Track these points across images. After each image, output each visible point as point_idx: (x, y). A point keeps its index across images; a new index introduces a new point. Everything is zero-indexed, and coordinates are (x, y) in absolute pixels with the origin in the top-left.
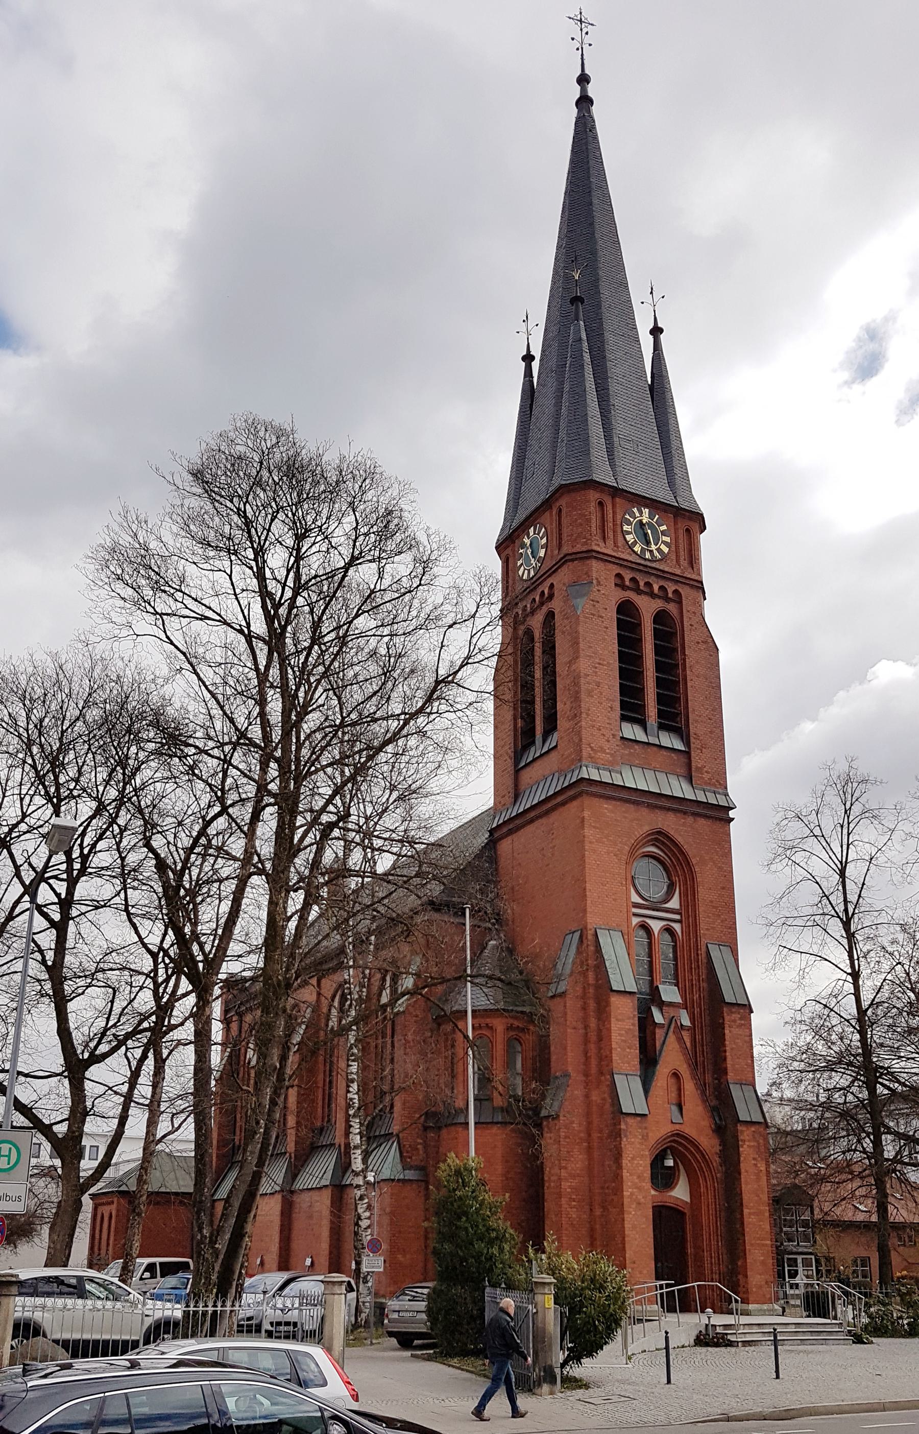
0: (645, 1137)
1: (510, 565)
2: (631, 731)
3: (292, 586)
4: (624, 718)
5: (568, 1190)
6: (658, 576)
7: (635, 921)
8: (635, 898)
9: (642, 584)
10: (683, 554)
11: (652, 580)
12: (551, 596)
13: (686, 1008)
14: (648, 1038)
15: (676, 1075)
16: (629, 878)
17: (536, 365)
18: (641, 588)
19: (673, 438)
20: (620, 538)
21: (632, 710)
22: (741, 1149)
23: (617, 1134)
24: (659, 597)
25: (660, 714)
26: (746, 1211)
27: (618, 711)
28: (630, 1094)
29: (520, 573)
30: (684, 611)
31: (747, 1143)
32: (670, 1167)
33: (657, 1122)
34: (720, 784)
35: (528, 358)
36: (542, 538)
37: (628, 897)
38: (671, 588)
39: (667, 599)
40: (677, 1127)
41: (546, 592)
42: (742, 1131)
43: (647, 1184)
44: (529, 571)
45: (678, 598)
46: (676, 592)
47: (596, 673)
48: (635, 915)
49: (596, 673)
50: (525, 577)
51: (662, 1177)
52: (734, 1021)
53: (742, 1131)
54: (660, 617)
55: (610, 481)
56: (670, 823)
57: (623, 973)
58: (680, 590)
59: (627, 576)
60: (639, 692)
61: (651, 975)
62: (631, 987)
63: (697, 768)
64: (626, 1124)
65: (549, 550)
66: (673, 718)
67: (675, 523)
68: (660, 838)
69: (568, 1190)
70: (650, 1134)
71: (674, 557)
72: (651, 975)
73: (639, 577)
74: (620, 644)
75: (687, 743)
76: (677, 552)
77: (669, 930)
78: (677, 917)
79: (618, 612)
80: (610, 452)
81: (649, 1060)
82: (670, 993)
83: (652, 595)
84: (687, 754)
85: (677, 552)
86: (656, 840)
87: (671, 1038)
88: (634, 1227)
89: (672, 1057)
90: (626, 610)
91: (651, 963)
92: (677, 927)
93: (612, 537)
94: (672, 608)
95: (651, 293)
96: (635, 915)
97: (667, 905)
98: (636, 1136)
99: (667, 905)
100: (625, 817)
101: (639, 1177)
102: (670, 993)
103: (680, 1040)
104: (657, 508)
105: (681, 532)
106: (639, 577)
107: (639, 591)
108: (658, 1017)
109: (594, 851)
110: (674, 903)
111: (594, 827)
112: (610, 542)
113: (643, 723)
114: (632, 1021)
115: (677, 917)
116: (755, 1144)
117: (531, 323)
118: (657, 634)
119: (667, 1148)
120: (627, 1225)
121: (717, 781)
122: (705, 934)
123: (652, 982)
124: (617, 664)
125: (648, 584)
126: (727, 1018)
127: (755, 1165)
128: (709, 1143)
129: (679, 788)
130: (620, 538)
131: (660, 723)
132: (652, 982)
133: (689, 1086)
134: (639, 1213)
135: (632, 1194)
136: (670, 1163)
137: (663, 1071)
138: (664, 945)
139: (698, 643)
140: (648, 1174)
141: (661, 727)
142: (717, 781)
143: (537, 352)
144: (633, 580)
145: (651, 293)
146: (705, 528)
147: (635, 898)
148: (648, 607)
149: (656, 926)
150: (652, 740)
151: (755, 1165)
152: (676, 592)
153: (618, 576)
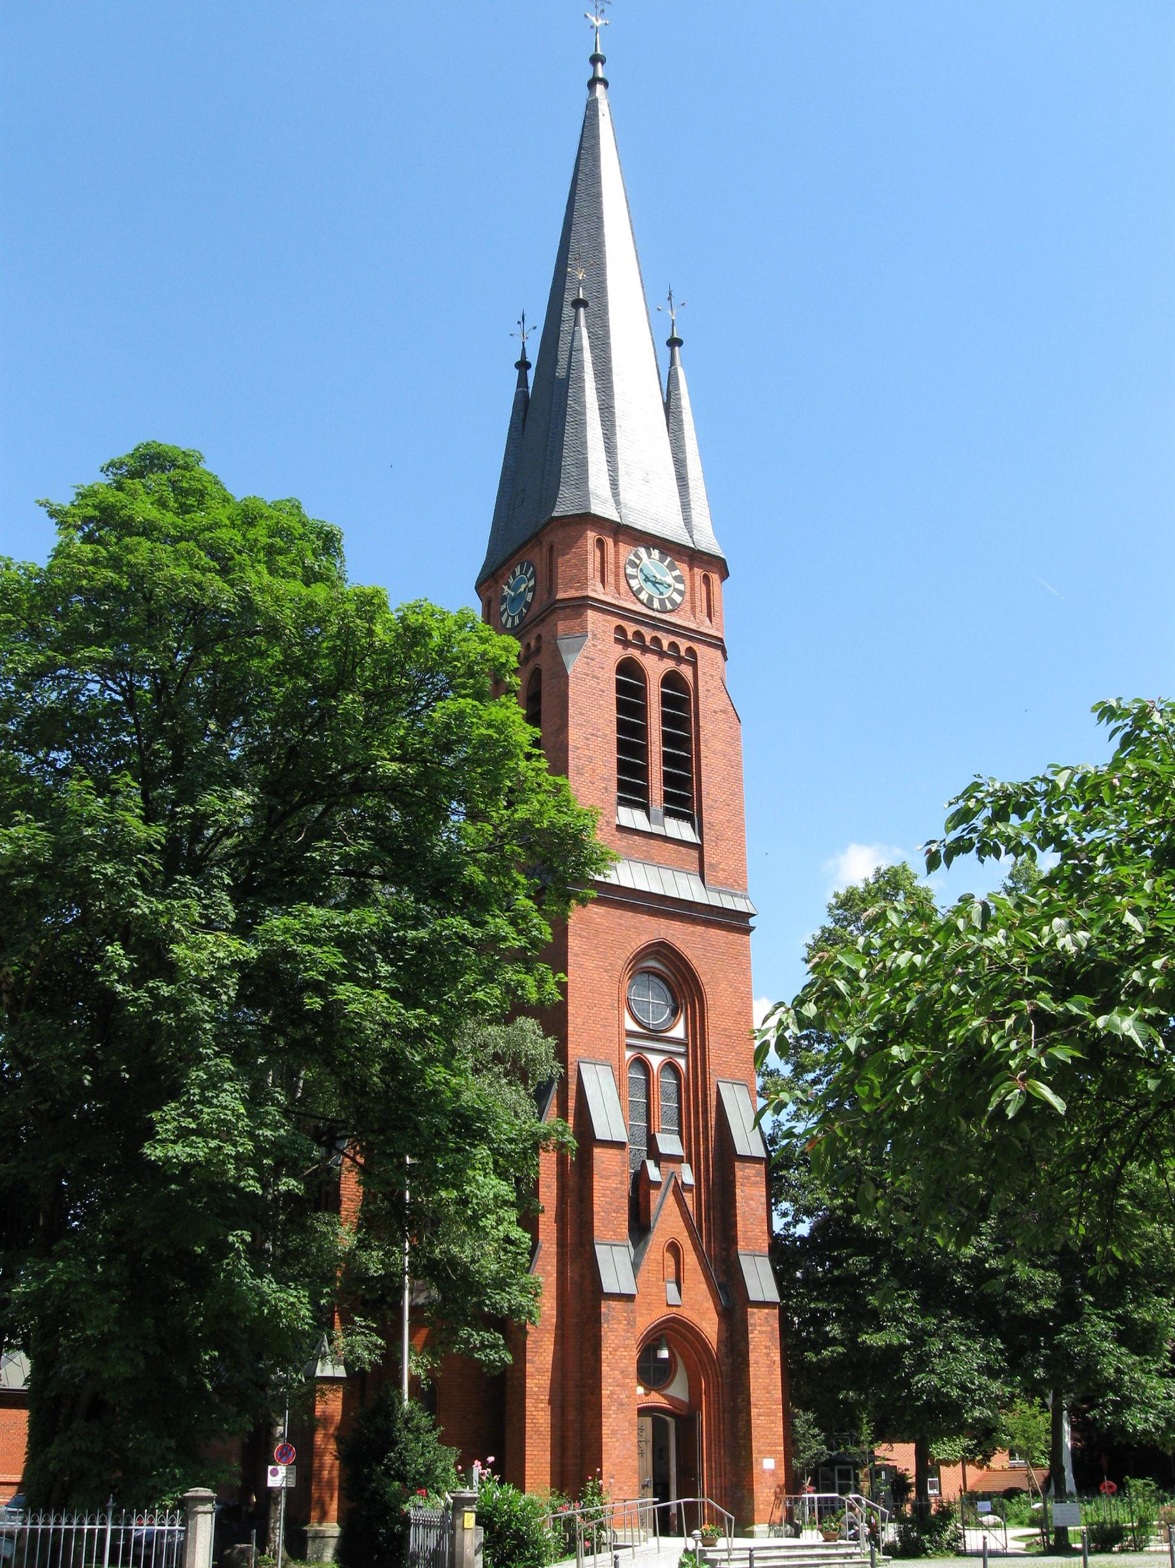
0: (631, 1323)
1: (493, 611)
2: (633, 818)
3: (773, 1295)
4: (622, 802)
5: (536, 1389)
6: (668, 631)
7: (629, 1054)
8: (634, 1027)
9: (648, 639)
10: (702, 604)
11: (660, 635)
12: (538, 650)
13: (690, 1162)
14: (641, 1199)
15: (674, 1248)
16: (623, 1000)
17: (531, 374)
18: (648, 643)
19: (567, 462)
20: (623, 583)
21: (632, 790)
22: (750, 1336)
23: (595, 1320)
24: (670, 657)
25: (668, 797)
26: (754, 1411)
27: (614, 793)
28: (615, 1267)
29: (504, 620)
30: (700, 673)
31: (758, 1328)
32: (665, 1359)
33: (649, 1304)
34: (739, 885)
35: (523, 365)
36: (529, 580)
37: (620, 1021)
38: (683, 644)
39: (679, 660)
40: (674, 1310)
41: (533, 644)
42: (753, 1314)
43: (632, 1380)
44: (513, 617)
45: (692, 658)
46: (690, 650)
47: (588, 745)
48: (629, 1046)
49: (588, 745)
50: (509, 625)
51: (652, 1373)
52: (748, 1178)
53: (753, 1314)
54: (671, 680)
55: (611, 513)
56: (677, 934)
57: (609, 1118)
58: (695, 648)
59: (631, 628)
60: (642, 772)
61: (648, 1121)
62: (621, 1135)
63: (711, 865)
64: (608, 1307)
65: (537, 593)
66: (683, 799)
67: (691, 569)
68: (662, 950)
69: (536, 1389)
70: (638, 1319)
71: (688, 608)
72: (648, 1121)
73: (644, 630)
74: (619, 711)
75: (701, 838)
76: (693, 602)
77: (671, 1067)
78: (682, 1050)
79: (618, 672)
80: (614, 484)
81: (640, 1226)
82: (669, 1144)
83: (662, 655)
84: (699, 848)
85: (693, 602)
86: (658, 953)
87: (671, 1199)
88: (614, 1433)
89: (668, 1222)
90: (627, 668)
91: (648, 1105)
92: (682, 1062)
93: (613, 581)
94: (686, 671)
95: (669, 299)
96: (629, 1046)
97: (669, 1034)
98: (620, 1322)
99: (669, 1034)
100: (620, 925)
101: (622, 1372)
102: (669, 1144)
103: (681, 1202)
104: (668, 549)
105: (698, 579)
106: (644, 630)
107: (644, 649)
108: (654, 1173)
109: (580, 966)
110: (679, 1032)
111: (580, 936)
112: (611, 588)
113: (645, 807)
114: (619, 1178)
115: (682, 1050)
116: (769, 1328)
117: (528, 324)
118: (666, 700)
119: (662, 1335)
120: (605, 1430)
121: (735, 881)
122: (715, 1070)
123: (649, 1128)
124: (615, 735)
125: (656, 640)
126: (739, 1174)
127: (768, 1355)
128: (709, 1326)
129: (687, 888)
130: (623, 583)
131: (666, 809)
132: (649, 1128)
133: (690, 1259)
134: (621, 1416)
135: (612, 1393)
136: (664, 1354)
137: (657, 1240)
138: (664, 1083)
139: (715, 712)
140: (633, 1369)
141: (669, 813)
142: (735, 881)
143: (533, 358)
144: (673, 645)
145: (669, 299)
146: (728, 575)
147: (634, 1027)
148: (655, 668)
149: (655, 1061)
150: (656, 829)
151: (768, 1355)
152: (690, 650)
153: (620, 630)
